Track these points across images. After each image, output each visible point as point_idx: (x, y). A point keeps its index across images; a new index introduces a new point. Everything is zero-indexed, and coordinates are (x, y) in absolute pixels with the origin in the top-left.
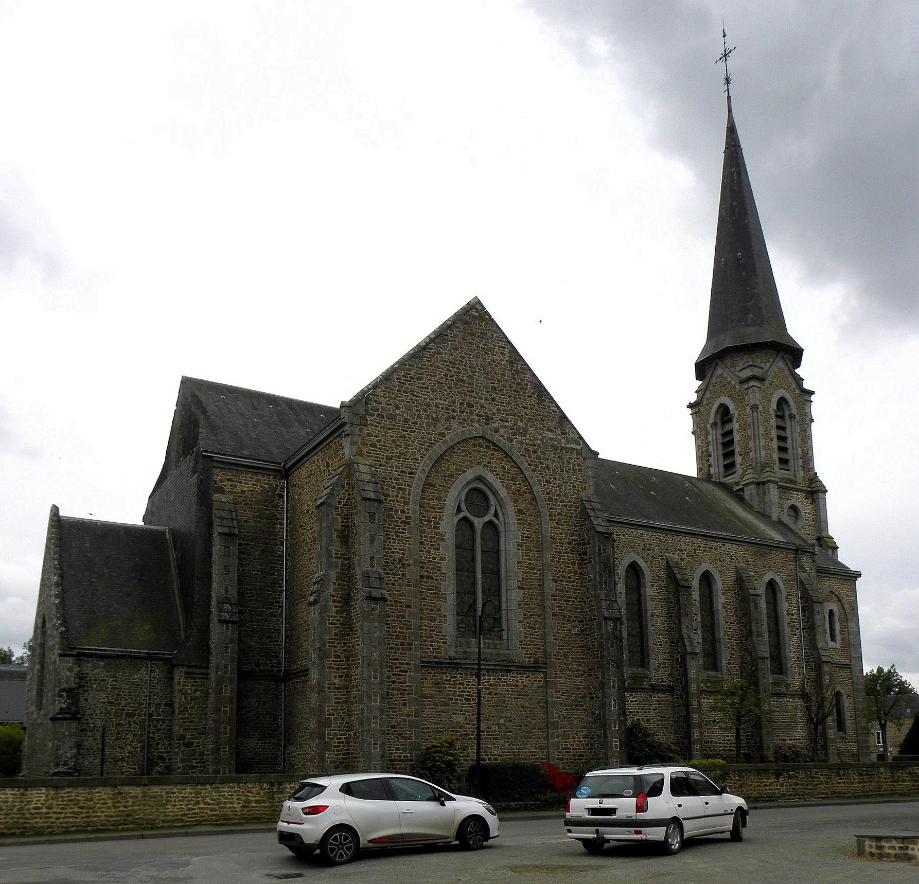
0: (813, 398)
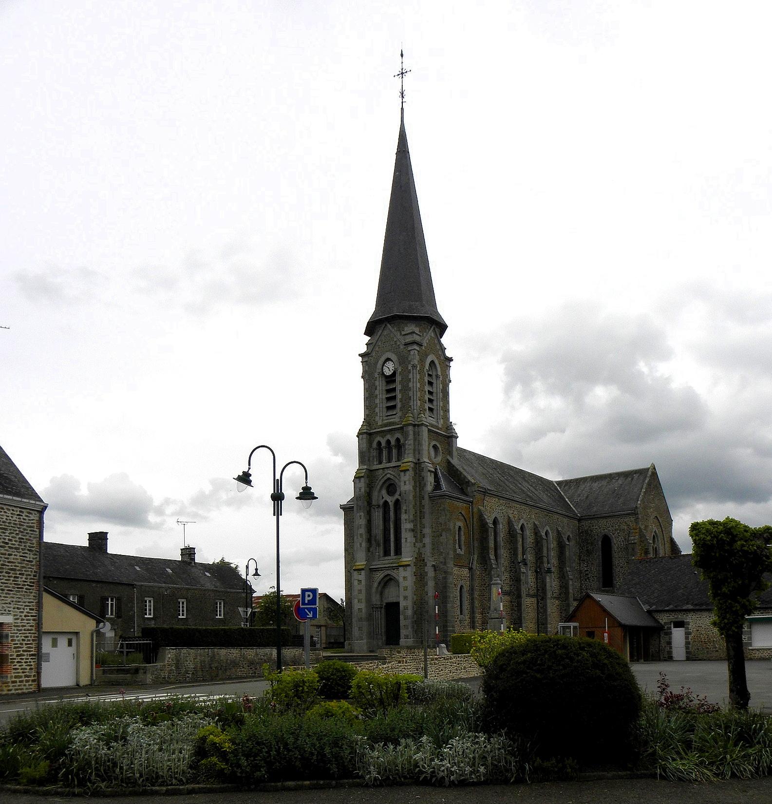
0: (452, 364)
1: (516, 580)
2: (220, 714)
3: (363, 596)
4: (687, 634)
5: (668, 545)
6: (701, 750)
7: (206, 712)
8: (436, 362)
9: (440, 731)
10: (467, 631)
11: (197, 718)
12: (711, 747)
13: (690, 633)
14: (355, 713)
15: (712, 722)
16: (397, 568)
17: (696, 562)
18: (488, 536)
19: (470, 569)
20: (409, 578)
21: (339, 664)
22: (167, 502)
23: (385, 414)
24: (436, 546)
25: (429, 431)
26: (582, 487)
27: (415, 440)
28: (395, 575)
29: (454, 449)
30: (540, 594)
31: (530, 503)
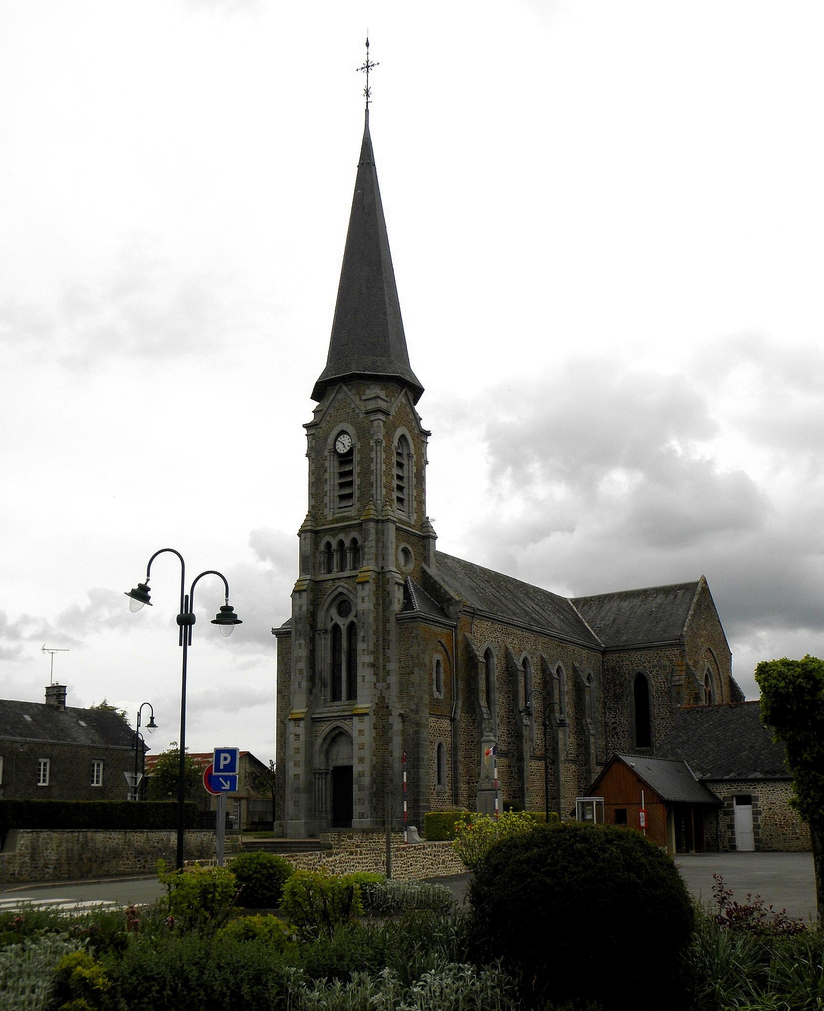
0: (429, 439)
1: (517, 735)
2: (92, 933)
3: (301, 757)
4: (756, 813)
5: (726, 689)
6: (780, 990)
7: (72, 929)
8: (408, 436)
9: (408, 959)
10: (448, 808)
11: (58, 940)
12: (793, 986)
13: (760, 813)
14: (287, 933)
15: (795, 948)
16: (350, 717)
17: (766, 717)
18: (477, 674)
19: (453, 720)
20: (367, 732)
21: (265, 856)
22: (26, 620)
23: (337, 505)
24: (404, 689)
25: (398, 529)
26: (607, 607)
27: (378, 541)
28: (346, 728)
29: (432, 554)
30: (550, 756)
31: (535, 629)
